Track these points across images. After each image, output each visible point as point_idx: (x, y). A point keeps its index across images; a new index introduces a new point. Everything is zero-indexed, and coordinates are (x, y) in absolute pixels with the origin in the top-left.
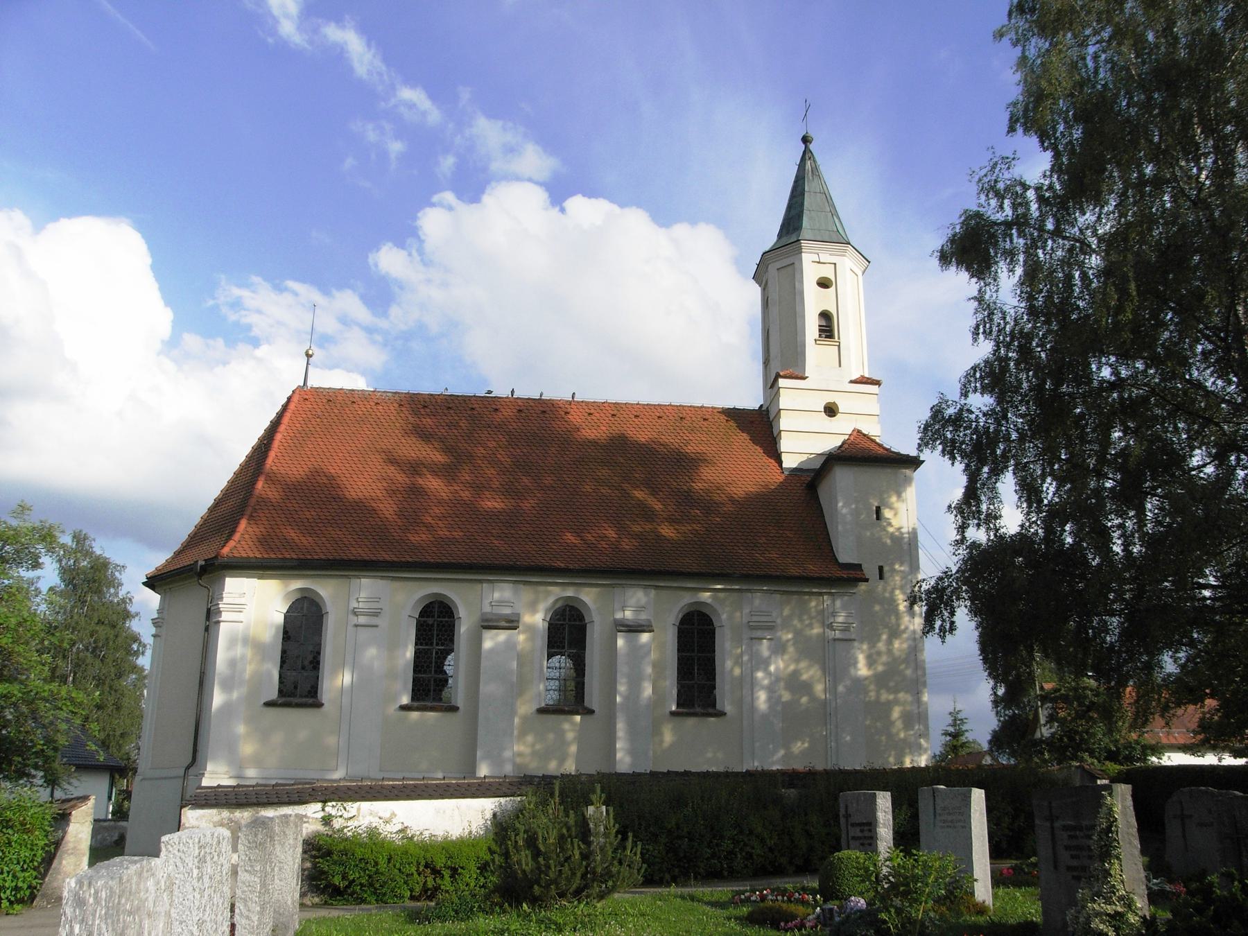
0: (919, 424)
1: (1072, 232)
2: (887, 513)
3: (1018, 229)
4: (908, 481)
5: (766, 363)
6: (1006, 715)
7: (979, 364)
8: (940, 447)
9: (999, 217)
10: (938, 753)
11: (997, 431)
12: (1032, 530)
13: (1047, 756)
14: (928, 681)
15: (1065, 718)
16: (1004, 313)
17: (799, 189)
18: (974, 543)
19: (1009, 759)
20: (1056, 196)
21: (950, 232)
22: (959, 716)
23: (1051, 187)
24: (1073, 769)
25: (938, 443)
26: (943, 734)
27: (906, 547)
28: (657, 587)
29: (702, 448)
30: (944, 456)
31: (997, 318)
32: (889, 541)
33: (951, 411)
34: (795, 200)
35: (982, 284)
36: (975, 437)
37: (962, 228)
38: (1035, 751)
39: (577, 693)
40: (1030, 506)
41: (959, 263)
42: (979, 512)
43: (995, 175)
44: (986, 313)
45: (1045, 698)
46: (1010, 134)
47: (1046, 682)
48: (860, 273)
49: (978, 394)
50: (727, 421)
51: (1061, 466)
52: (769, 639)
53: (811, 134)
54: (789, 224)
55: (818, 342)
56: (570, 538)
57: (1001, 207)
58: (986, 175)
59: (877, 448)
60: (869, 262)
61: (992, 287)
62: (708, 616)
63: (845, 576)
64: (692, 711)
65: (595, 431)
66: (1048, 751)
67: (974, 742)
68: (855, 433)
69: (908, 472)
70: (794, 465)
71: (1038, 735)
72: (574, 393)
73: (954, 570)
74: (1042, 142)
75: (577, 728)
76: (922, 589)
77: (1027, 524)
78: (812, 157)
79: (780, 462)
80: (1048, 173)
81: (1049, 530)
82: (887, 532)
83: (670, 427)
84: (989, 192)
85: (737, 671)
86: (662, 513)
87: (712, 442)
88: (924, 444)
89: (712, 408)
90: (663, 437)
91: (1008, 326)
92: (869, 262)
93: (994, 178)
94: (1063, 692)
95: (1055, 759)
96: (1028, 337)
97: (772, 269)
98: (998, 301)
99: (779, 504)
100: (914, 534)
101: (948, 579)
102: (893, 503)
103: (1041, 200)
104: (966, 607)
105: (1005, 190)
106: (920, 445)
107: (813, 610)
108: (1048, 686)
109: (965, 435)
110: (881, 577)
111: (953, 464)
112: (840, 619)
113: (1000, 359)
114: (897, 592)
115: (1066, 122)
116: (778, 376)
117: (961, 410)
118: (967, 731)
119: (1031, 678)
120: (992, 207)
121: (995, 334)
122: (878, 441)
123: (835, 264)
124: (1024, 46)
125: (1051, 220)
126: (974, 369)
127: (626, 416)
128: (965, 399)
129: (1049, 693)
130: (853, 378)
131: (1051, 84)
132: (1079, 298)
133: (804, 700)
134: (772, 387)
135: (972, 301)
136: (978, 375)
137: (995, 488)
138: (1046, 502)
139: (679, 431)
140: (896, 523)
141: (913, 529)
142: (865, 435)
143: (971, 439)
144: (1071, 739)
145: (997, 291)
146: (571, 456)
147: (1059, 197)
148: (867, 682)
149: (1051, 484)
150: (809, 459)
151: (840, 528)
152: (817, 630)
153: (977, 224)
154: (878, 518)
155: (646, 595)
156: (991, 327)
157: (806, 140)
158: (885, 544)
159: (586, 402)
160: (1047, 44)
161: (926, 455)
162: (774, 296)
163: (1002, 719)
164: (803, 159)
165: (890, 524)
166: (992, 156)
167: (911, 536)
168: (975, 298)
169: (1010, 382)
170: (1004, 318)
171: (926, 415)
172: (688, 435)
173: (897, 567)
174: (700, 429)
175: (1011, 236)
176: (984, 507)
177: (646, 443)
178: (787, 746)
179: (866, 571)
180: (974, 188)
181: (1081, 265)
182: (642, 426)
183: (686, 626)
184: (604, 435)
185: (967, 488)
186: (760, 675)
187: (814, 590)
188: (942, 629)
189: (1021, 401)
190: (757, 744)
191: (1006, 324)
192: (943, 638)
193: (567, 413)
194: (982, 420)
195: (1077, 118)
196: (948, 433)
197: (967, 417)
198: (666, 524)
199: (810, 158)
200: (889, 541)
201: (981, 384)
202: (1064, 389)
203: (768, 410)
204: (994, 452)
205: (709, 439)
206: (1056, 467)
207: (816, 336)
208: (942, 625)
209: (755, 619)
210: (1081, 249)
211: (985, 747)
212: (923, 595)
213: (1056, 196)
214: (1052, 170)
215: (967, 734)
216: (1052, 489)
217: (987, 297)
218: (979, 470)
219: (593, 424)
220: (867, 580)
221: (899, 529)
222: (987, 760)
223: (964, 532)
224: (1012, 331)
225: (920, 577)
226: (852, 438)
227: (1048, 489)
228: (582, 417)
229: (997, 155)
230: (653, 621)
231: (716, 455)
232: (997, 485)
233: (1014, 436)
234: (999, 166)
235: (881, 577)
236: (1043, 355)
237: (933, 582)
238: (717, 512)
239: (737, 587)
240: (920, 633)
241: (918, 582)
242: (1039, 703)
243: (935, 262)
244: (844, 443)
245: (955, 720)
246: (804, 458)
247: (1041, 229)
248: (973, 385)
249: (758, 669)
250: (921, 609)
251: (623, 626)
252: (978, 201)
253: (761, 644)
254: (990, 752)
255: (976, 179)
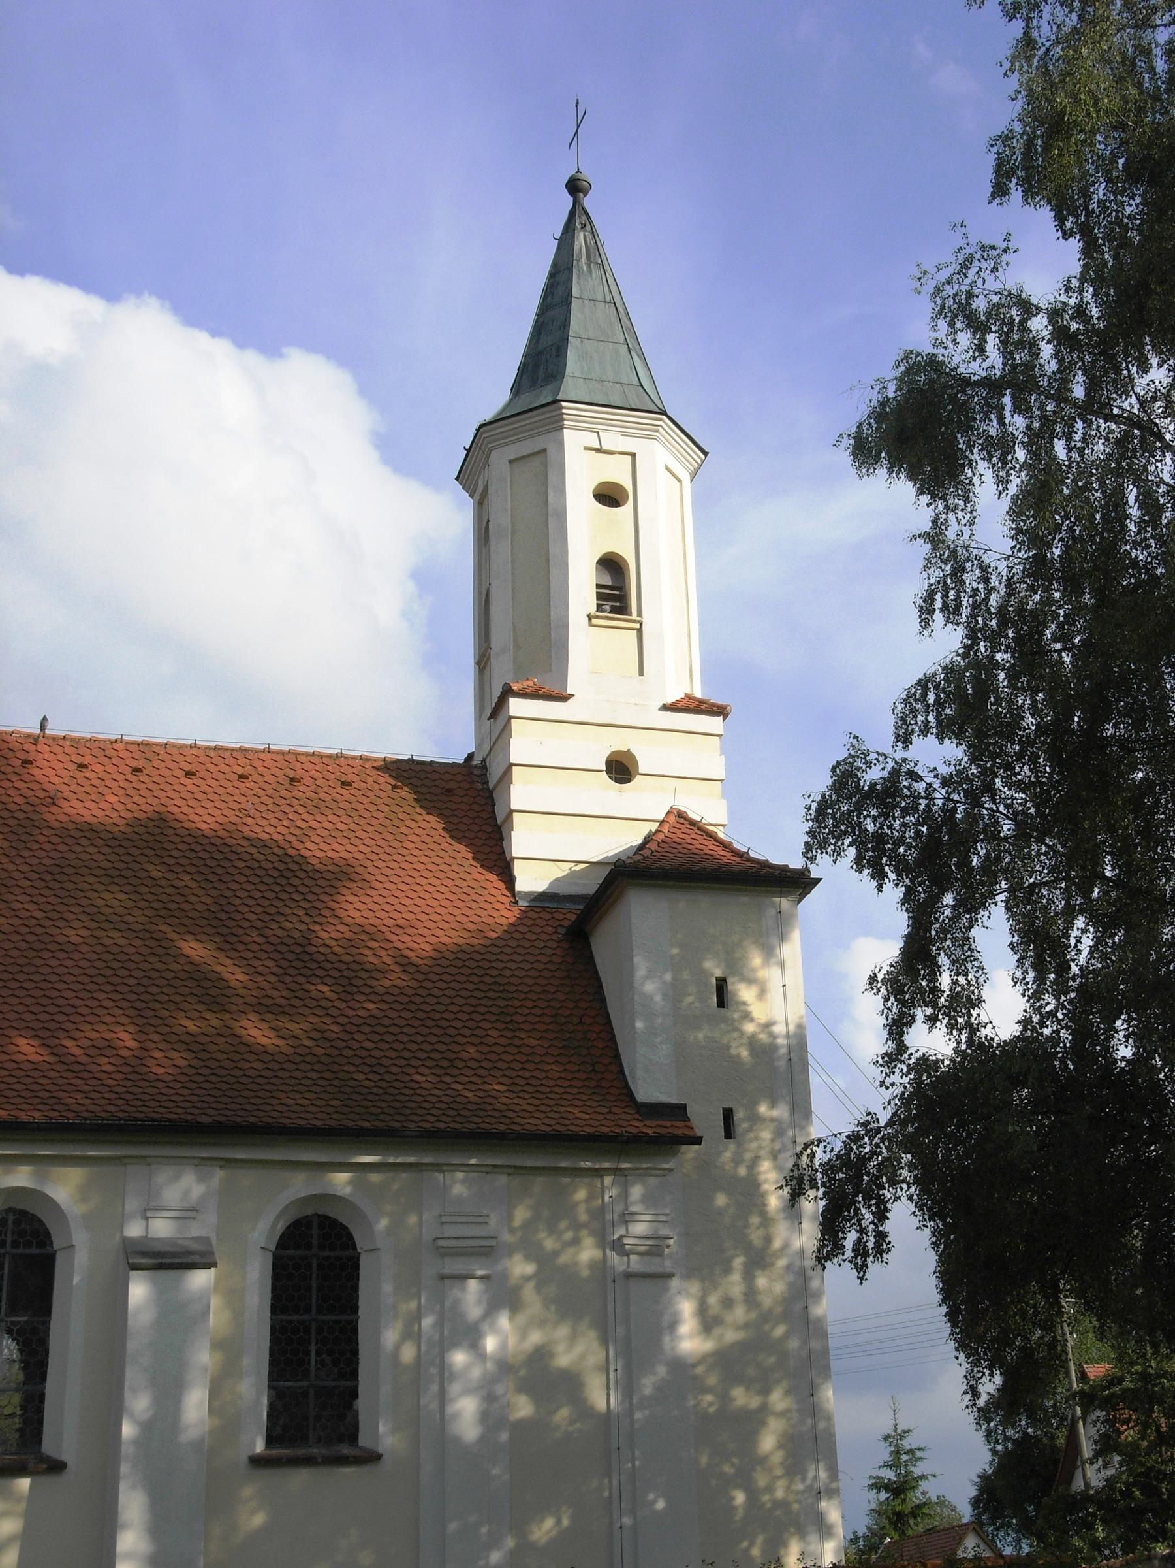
0: (808, 802)
1: (1126, 405)
2: (745, 993)
3: (1014, 398)
4: (781, 927)
5: (483, 662)
6: (1007, 1439)
7: (934, 675)
8: (852, 852)
9: (975, 369)
10: (862, 1531)
11: (972, 818)
12: (1047, 1032)
13: (1100, 1534)
14: (835, 1366)
15: (1134, 1445)
16: (984, 569)
17: (560, 292)
18: (924, 1059)
19: (1018, 1542)
20: (1091, 331)
21: (875, 397)
22: (907, 1444)
23: (1080, 312)
24: (1156, 1562)
25: (848, 841)
26: (871, 1487)
27: (782, 1064)
28: (227, 1162)
29: (339, 850)
30: (860, 870)
31: (971, 579)
32: (745, 1053)
33: (874, 775)
34: (550, 313)
35: (941, 507)
36: (924, 829)
37: (899, 388)
38: (1074, 1522)
39: (25, 1422)
40: (1040, 979)
41: (894, 465)
42: (935, 991)
43: (967, 281)
44: (948, 568)
45: (1089, 1398)
46: (998, 200)
47: (1092, 1361)
48: (685, 477)
49: (931, 739)
50: (394, 787)
51: (1105, 893)
52: (481, 1278)
53: (586, 174)
54: (536, 366)
55: (595, 621)
56: (27, 1048)
57: (981, 349)
58: (949, 282)
59: (720, 851)
60: (706, 454)
61: (960, 514)
62: (345, 1228)
63: (650, 1131)
64: (300, 1452)
65: (92, 805)
66: (1104, 1521)
67: (942, 1502)
68: (672, 819)
69: (784, 903)
70: (540, 886)
71: (1078, 1485)
72: (45, 719)
73: (884, 1118)
74: (1060, 220)
75: (22, 1506)
76: (817, 1162)
77: (1036, 1019)
78: (588, 224)
79: (509, 880)
80: (1075, 283)
81: (1083, 1033)
82: (742, 1033)
83: (264, 799)
84: (956, 316)
85: (408, 1353)
86: (242, 992)
87: (360, 834)
88: (816, 843)
89: (361, 758)
90: (249, 821)
91: (993, 597)
92: (706, 454)
93: (964, 288)
94: (1127, 1384)
95: (1119, 1539)
96: (1037, 620)
97: (499, 460)
98: (973, 544)
99: (507, 973)
100: (798, 1043)
101: (872, 1138)
102: (754, 970)
103: (1061, 336)
104: (910, 1198)
105: (988, 314)
106: (808, 847)
107: (582, 1208)
108: (1095, 1372)
109: (904, 825)
110: (729, 1134)
111: (880, 888)
112: (639, 1228)
113: (976, 665)
114: (765, 1166)
115: (1109, 181)
116: (507, 692)
117: (895, 773)
118: (923, 1477)
119: (1056, 1357)
120: (961, 348)
121: (965, 612)
122: (721, 835)
123: (633, 455)
124: (1028, 20)
125: (1080, 378)
126: (923, 684)
127: (167, 773)
128: (905, 747)
129: (1098, 1387)
130: (671, 699)
131: (1077, 101)
132: (1136, 544)
133: (564, 1413)
134: (494, 714)
135: (920, 541)
136: (931, 698)
137: (968, 939)
138: (1075, 969)
139: (287, 809)
140: (759, 1012)
141: (800, 1027)
142: (693, 823)
143: (918, 834)
144: (1150, 1491)
145: (971, 523)
146: (34, 861)
147: (1097, 332)
148: (699, 1370)
149: (1084, 931)
150: (572, 874)
151: (639, 1025)
152: (588, 1253)
153: (931, 382)
154: (721, 1003)
155: (201, 1179)
156: (958, 597)
157: (575, 187)
158: (736, 1061)
159: (73, 739)
160: (1074, 16)
161: (822, 867)
162: (500, 519)
163: (999, 1448)
164: (569, 228)
165: (747, 1016)
166: (962, 243)
167: (793, 1042)
168: (925, 536)
169: (998, 714)
170: (986, 580)
171: (821, 783)
172: (305, 816)
173: (763, 1109)
174: (333, 805)
175: (1000, 409)
176: (945, 980)
177: (211, 834)
178: (519, 1528)
179: (695, 1121)
180: (927, 307)
181: (1139, 479)
182: (201, 796)
183: (291, 1252)
184: (114, 815)
185: (910, 939)
186: (459, 1358)
187: (583, 1164)
188: (860, 1250)
189: (1020, 756)
190: (453, 1526)
191: (989, 591)
192: (861, 1268)
193: (26, 763)
194: (940, 795)
195: (1132, 175)
196: (869, 820)
197: (909, 788)
198: (252, 1016)
199: (583, 227)
200: (745, 1053)
201: (937, 718)
202: (1109, 730)
203: (484, 766)
204: (965, 862)
205: (353, 826)
206: (1096, 893)
207: (591, 605)
208: (859, 1240)
209: (449, 1231)
210: (1143, 440)
211: (966, 1513)
212: (819, 1175)
213: (1091, 331)
214: (1083, 279)
215: (924, 1485)
216: (1087, 942)
217: (951, 534)
218: (934, 900)
219: (88, 789)
220: (697, 1141)
221: (768, 1025)
222: (970, 1546)
223: (901, 1034)
224: (1002, 608)
225: (815, 1132)
226: (666, 829)
227: (1079, 941)
228: (64, 773)
229: (973, 240)
230: (214, 1242)
231: (368, 863)
232: (974, 932)
233: (1007, 827)
234: (976, 263)
235: (729, 1134)
236: (1066, 658)
237: (838, 1145)
238: (367, 990)
239: (411, 1159)
240: (810, 1262)
241: (806, 1146)
242: (1078, 1410)
243: (844, 457)
244: (648, 839)
245: (897, 1453)
246: (562, 871)
247: (1062, 395)
248: (920, 718)
249: (455, 1345)
250: (813, 1205)
251: (144, 1254)
252: (935, 335)
253: (463, 1289)
254: (977, 1526)
255: (930, 287)
